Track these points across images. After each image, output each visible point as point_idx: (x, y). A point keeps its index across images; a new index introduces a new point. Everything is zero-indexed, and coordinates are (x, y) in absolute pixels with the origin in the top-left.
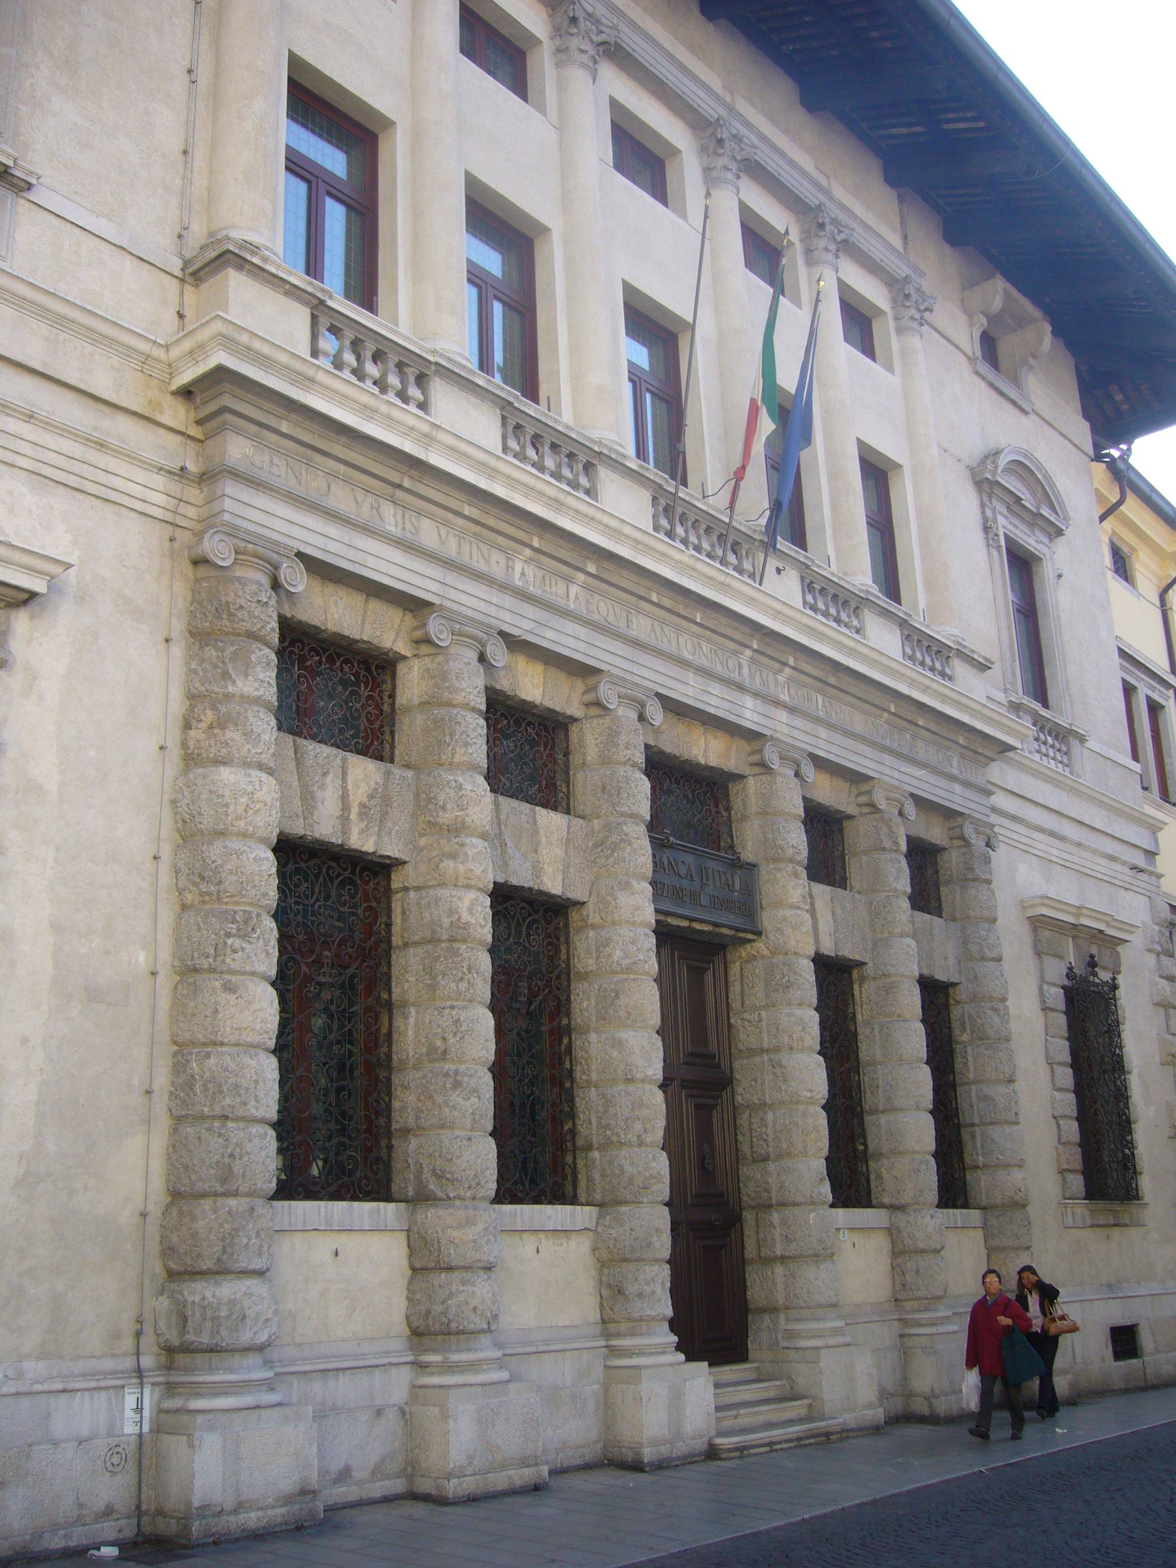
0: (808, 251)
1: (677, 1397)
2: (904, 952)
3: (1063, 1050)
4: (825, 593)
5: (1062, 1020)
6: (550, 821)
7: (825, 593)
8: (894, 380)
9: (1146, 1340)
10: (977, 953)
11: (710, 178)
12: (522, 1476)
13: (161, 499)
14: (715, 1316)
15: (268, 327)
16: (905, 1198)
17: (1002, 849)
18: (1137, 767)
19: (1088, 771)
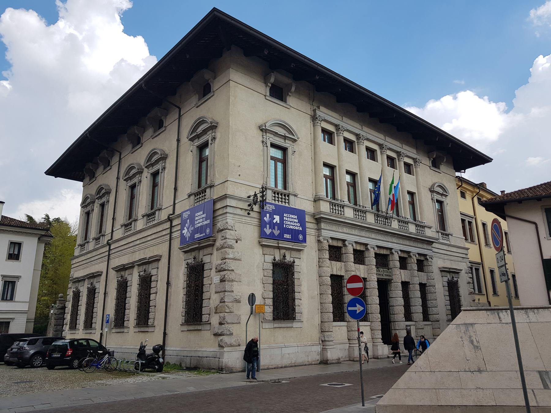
0: (398, 159)
2: (417, 278)
6: (362, 266)
7: (404, 222)
11: (382, 153)
15: (325, 207)
19: (452, 241)
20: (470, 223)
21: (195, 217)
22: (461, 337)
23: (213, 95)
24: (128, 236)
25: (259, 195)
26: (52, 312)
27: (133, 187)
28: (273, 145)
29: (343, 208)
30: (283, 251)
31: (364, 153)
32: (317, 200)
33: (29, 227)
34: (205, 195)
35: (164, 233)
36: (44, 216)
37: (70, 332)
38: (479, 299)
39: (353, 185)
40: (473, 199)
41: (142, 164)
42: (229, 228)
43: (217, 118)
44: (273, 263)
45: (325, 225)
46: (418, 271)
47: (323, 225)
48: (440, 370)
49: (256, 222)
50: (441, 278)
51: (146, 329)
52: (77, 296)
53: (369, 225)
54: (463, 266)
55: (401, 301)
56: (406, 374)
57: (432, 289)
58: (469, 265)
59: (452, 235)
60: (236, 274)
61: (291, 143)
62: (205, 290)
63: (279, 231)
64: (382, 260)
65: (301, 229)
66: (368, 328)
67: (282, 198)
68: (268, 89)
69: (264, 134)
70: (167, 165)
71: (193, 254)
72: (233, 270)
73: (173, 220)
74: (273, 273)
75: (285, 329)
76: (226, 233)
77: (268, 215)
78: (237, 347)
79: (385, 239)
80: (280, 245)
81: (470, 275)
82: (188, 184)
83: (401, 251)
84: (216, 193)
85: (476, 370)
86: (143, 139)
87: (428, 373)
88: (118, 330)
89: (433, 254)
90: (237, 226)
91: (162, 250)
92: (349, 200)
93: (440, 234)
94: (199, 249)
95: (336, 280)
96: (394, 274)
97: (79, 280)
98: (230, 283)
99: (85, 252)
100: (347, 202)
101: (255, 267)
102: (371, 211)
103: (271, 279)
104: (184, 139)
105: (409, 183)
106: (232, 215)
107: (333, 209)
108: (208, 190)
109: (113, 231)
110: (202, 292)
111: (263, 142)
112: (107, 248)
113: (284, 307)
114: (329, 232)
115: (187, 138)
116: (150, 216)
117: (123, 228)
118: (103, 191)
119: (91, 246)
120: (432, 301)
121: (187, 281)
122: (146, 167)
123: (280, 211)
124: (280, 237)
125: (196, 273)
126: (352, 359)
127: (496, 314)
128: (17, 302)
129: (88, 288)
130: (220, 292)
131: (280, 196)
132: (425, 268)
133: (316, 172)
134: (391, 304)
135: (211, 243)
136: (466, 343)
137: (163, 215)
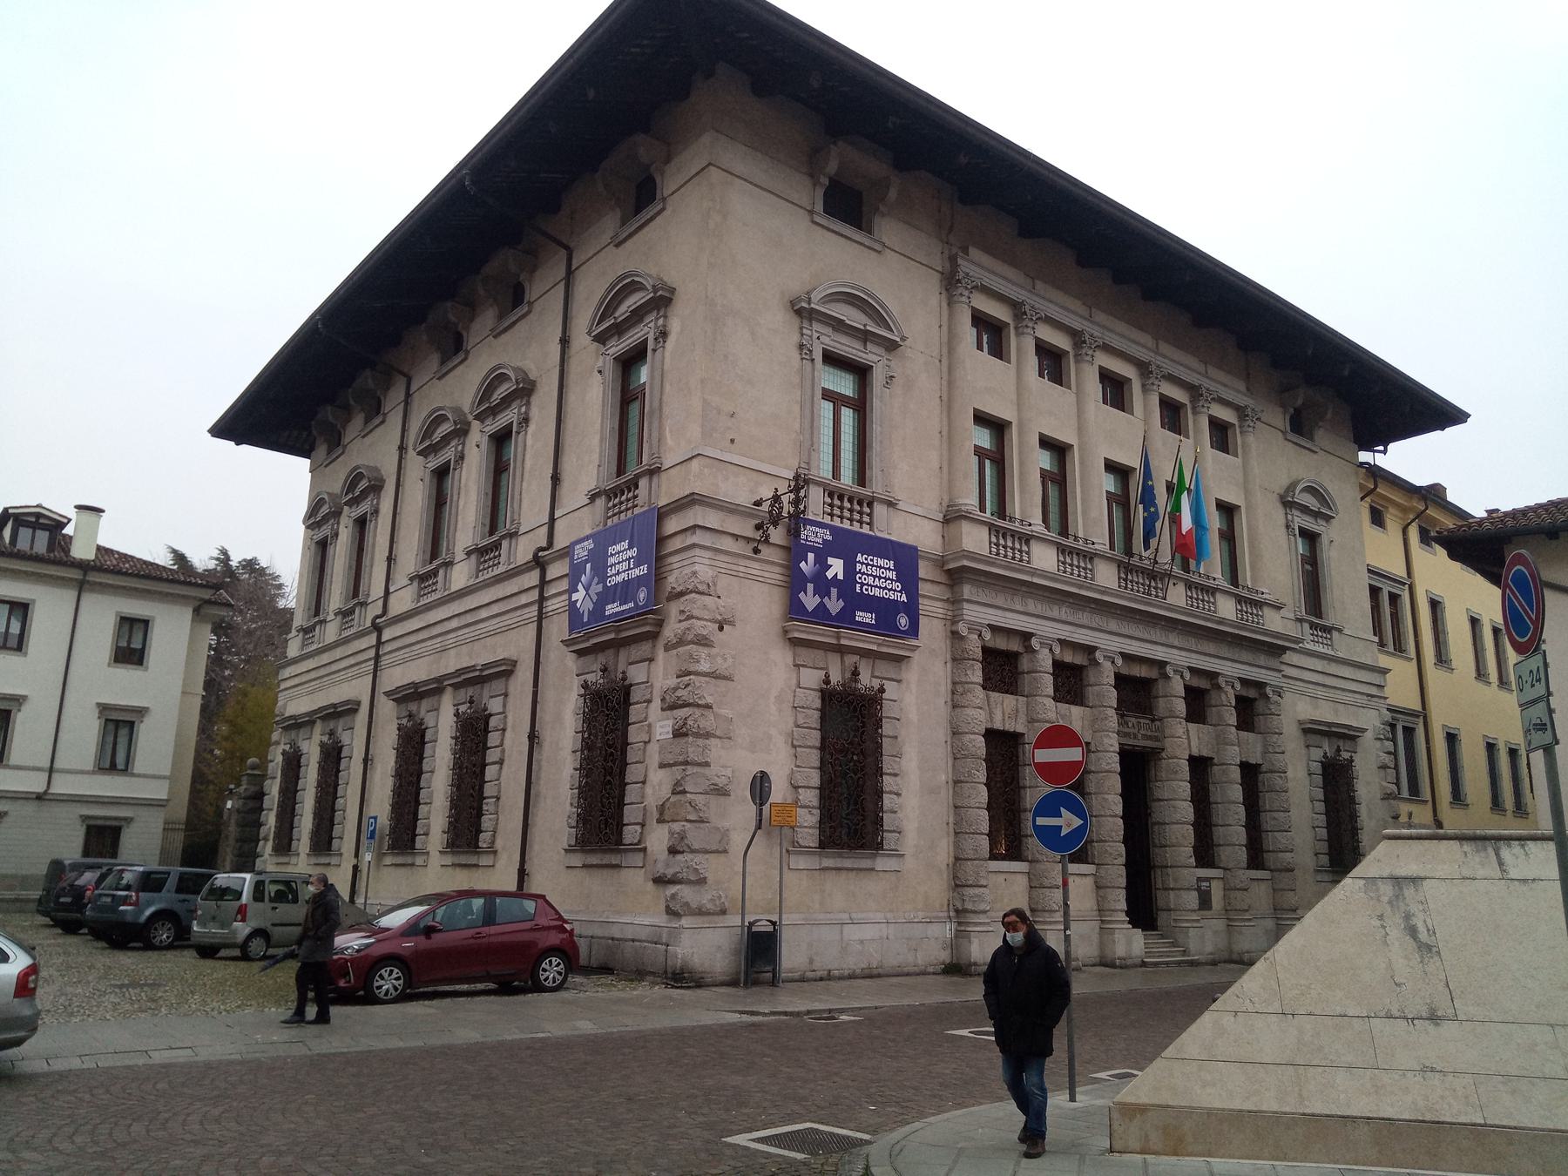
0: (1194, 408)
1: (1129, 942)
2: (1236, 748)
3: (1319, 794)
8: (1239, 461)
11: (1145, 389)
14: (1143, 912)
15: (975, 539)
20: (1394, 598)
21: (606, 556)
22: (1381, 917)
23: (663, 209)
24: (429, 608)
25: (785, 499)
26: (229, 804)
27: (442, 473)
28: (831, 359)
29: (1027, 542)
30: (851, 659)
31: (1094, 388)
32: (952, 517)
33: (176, 580)
34: (635, 497)
35: (524, 599)
36: (216, 553)
37: (275, 860)
38: (1410, 815)
39: (1057, 479)
40: (1405, 531)
41: (466, 409)
42: (702, 588)
43: (672, 277)
44: (822, 691)
45: (974, 590)
46: (1238, 728)
48: (1311, 1009)
49: (775, 574)
50: (1304, 751)
51: (472, 860)
52: (293, 763)
53: (1103, 593)
54: (1369, 720)
55: (1186, 811)
56: (1207, 1018)
57: (1278, 781)
58: (1388, 716)
59: (1340, 631)
60: (716, 716)
61: (881, 351)
63: (841, 603)
64: (1137, 692)
65: (904, 598)
66: (1089, 881)
67: (851, 510)
68: (820, 193)
70: (535, 412)
71: (602, 659)
72: (708, 707)
73: (548, 563)
74: (823, 719)
75: (852, 875)
77: (811, 556)
78: (716, 918)
79: (1146, 636)
80: (843, 642)
81: (1389, 745)
82: (588, 465)
83: (1191, 669)
84: (667, 490)
85: (1424, 1015)
86: (471, 340)
87: (1274, 1018)
88: (399, 860)
89: (1282, 682)
90: (723, 582)
91: (519, 645)
92: (1045, 520)
93: (1306, 626)
94: (618, 645)
95: (1003, 746)
96: (1168, 732)
97: (298, 724)
98: (700, 742)
99: (314, 647)
100: (1038, 526)
101: (772, 699)
102: (1109, 553)
103: (817, 734)
104: (581, 339)
105: (1221, 477)
106: (708, 554)
107: (997, 545)
108: (643, 483)
109: (387, 593)
110: (624, 764)
111: (801, 346)
112: (372, 639)
113: (850, 812)
114: (984, 613)
115: (589, 333)
116: (483, 553)
117: (415, 584)
118: (363, 484)
119: (331, 632)
120: (1275, 815)
121: (583, 732)
122: (477, 417)
123: (846, 545)
124: (845, 619)
125: (608, 712)
127: (1490, 850)
128: (139, 776)
129: (322, 745)
130: (675, 764)
131: (847, 505)
132: (1260, 722)
133: (950, 438)
134: (1156, 817)
135: (647, 628)
136: (1396, 933)
137: (523, 551)
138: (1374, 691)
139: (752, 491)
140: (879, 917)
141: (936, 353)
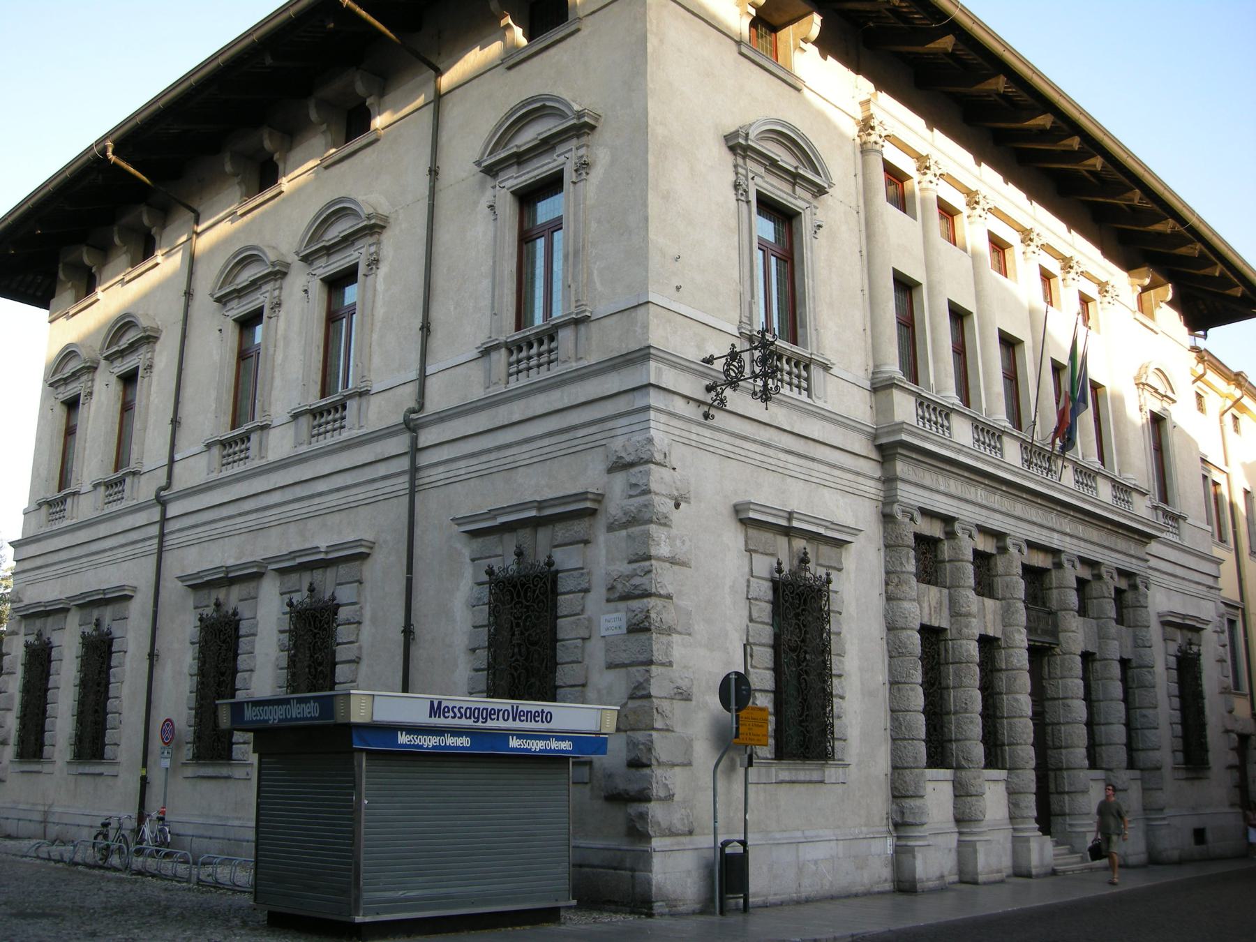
4: (1085, 473)
5: (1174, 673)
9: (1209, 836)
10: (1140, 644)
12: (997, 876)
13: (873, 491)
15: (904, 408)
16: (1113, 765)
17: (1152, 587)
18: (1209, 528)
25: (746, 357)
30: (799, 544)
32: (880, 387)
44: (773, 581)
47: (901, 468)
61: (808, 196)
62: (561, 655)
69: (740, 161)
72: (669, 597)
76: (648, 473)
78: (682, 839)
80: (795, 524)
90: (678, 455)
93: (1160, 513)
98: (664, 639)
101: (727, 589)
106: (663, 418)
111: (736, 186)
126: (968, 878)
135: (589, 504)
137: (379, 413)
138: (1210, 581)
139: (699, 347)
140: (827, 833)
141: (853, 204)
